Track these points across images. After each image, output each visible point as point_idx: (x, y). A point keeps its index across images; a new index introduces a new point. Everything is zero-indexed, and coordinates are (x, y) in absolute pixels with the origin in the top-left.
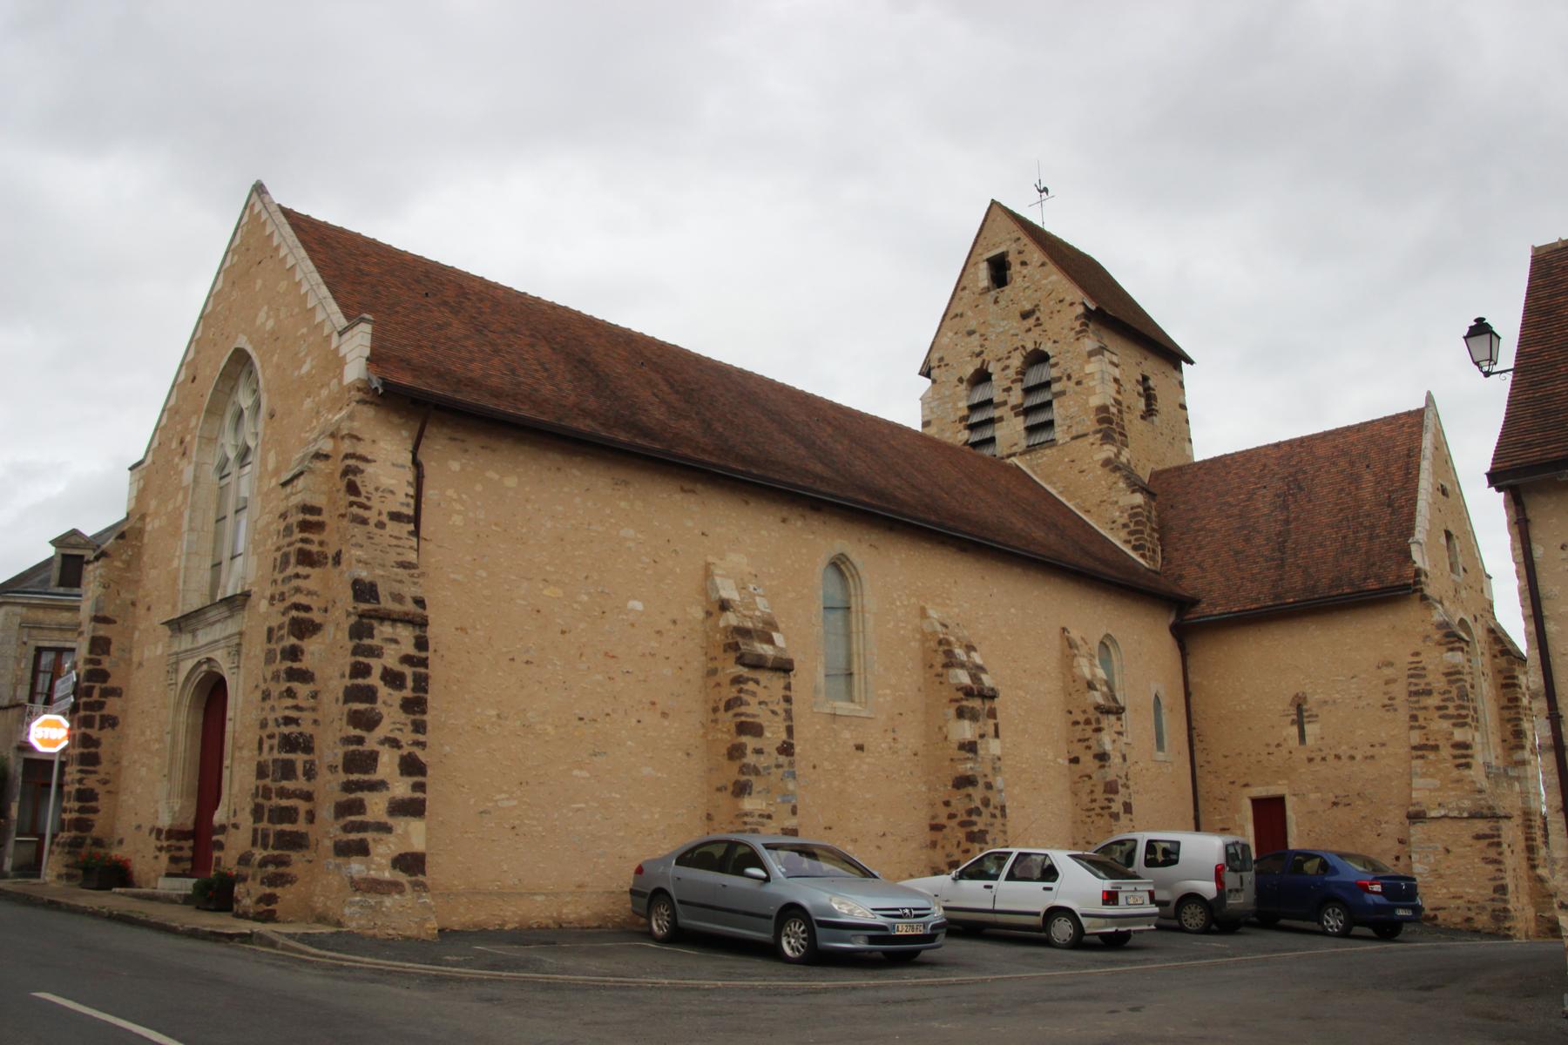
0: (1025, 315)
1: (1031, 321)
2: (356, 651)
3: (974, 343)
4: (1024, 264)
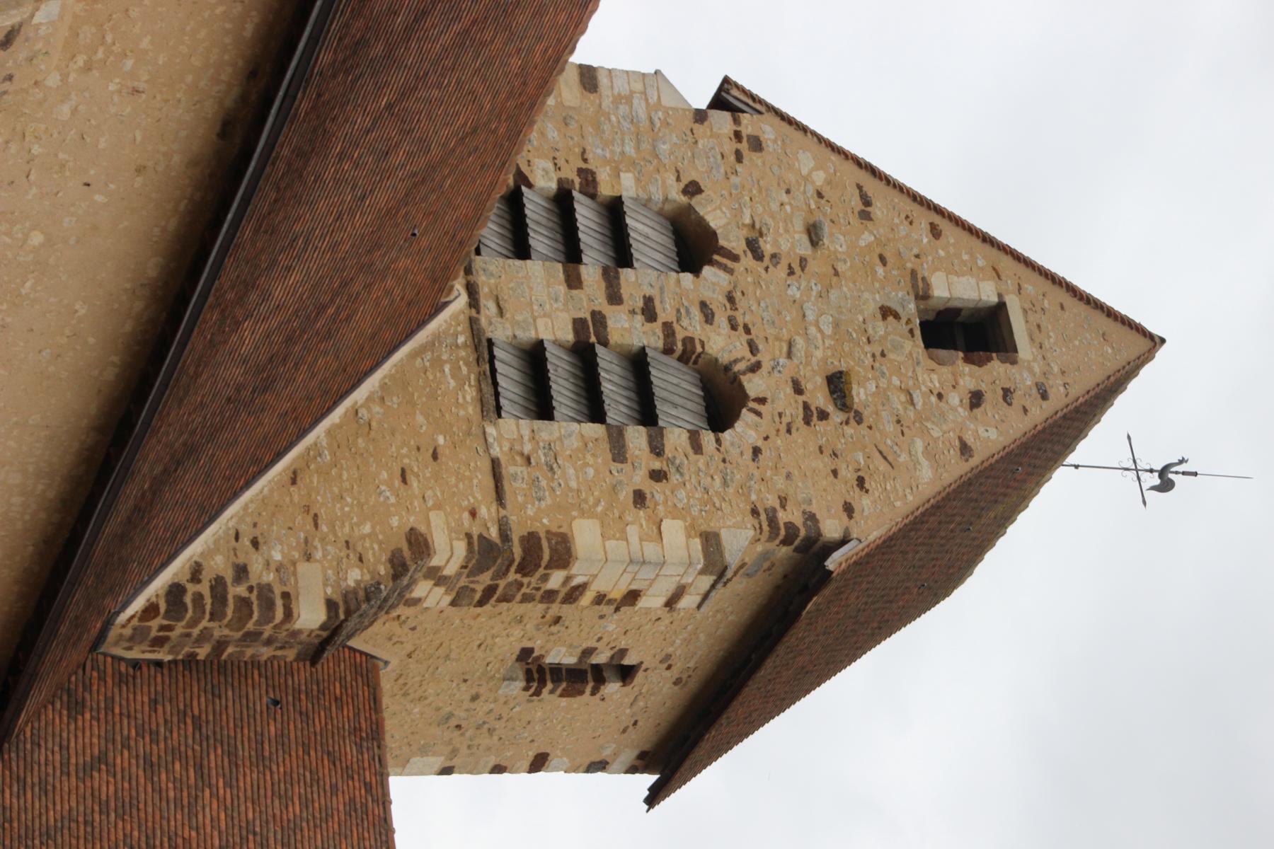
0: (837, 384)
1: (820, 398)
3: (787, 240)
4: (976, 399)
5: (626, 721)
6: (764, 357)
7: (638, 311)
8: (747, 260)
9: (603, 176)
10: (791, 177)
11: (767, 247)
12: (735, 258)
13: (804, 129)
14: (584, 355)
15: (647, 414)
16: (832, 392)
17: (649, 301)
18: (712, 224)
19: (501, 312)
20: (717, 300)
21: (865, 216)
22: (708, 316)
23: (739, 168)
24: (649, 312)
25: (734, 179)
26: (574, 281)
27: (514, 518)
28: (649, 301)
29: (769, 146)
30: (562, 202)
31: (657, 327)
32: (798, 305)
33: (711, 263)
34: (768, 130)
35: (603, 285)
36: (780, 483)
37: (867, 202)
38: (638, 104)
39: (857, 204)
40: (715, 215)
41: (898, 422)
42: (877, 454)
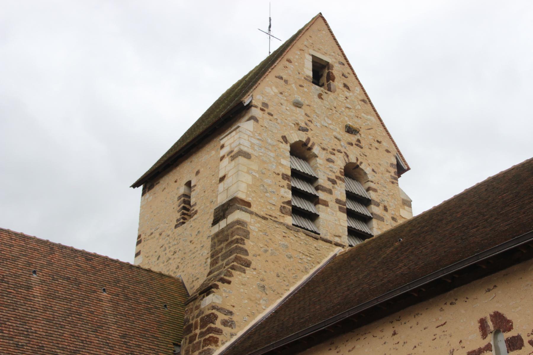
0: (350, 130)
1: (353, 138)
3: (299, 115)
4: (345, 86)
7: (333, 185)
8: (310, 134)
11: (303, 125)
12: (309, 139)
16: (352, 133)
17: (329, 179)
18: (298, 140)
19: (339, 237)
21: (286, 82)
23: (275, 117)
25: (279, 121)
27: (254, 263)
28: (329, 179)
30: (296, 192)
33: (310, 149)
35: (325, 193)
36: (382, 169)
37: (281, 78)
39: (282, 82)
40: (295, 137)
41: (357, 117)
42: (369, 131)
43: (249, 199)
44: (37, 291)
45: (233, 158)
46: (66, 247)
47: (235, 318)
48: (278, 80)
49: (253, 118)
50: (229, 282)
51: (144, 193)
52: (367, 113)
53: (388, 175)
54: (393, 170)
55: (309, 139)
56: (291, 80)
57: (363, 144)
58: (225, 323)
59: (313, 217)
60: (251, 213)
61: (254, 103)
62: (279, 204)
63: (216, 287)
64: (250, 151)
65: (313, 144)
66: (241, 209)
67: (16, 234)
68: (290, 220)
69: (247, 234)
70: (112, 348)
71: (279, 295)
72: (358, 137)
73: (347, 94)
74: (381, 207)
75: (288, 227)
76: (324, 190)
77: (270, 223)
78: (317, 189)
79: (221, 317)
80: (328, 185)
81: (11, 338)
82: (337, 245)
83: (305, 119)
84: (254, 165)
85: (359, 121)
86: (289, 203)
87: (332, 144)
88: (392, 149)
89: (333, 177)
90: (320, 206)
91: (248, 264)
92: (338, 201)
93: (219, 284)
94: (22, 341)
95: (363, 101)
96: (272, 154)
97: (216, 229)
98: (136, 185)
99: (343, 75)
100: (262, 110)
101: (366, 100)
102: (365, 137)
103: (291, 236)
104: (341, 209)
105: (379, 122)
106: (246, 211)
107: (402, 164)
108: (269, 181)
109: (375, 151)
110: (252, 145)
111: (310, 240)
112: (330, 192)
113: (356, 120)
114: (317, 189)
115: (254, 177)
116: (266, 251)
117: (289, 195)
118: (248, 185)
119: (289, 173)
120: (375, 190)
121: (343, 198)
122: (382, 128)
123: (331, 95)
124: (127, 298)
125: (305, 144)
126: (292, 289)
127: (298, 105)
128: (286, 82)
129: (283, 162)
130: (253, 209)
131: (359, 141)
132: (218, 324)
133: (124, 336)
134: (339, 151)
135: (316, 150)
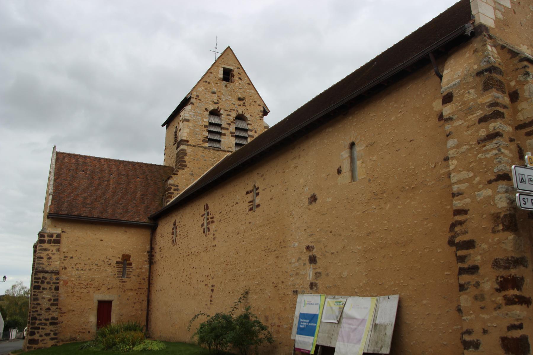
0: (240, 99)
1: (241, 103)
2: (58, 296)
3: (215, 98)
4: (240, 78)
5: (181, 131)
6: (235, 109)
8: (219, 105)
9: (205, 124)
10: (203, 93)
11: (216, 101)
12: (218, 107)
13: (194, 87)
14: (237, 137)
15: (246, 130)
17: (227, 124)
20: (226, 113)
21: (209, 83)
22: (229, 115)
24: (229, 124)
26: (225, 135)
28: (227, 124)
29: (198, 94)
30: (210, 132)
31: (232, 124)
32: (226, 100)
33: (219, 111)
34: (194, 95)
36: (256, 114)
37: (206, 82)
38: (191, 113)
39: (207, 84)
40: (211, 108)
43: (188, 139)
44: (111, 182)
45: (183, 122)
46: (126, 161)
47: (179, 188)
48: (205, 83)
49: (192, 104)
50: (177, 174)
51: (167, 127)
52: (250, 89)
53: (258, 116)
54: (261, 114)
55: (218, 107)
56: (211, 81)
57: (246, 104)
58: (175, 190)
59: (219, 141)
60: (188, 145)
61: (192, 96)
62: (203, 138)
63: (172, 177)
64: (189, 118)
65: (221, 109)
66: (183, 144)
67: (107, 159)
68: (207, 145)
69: (185, 154)
70: (136, 201)
71: (199, 176)
72: (244, 101)
73: (240, 82)
74: (253, 131)
75: (205, 148)
76: (224, 129)
77: (197, 148)
78: (221, 129)
79: (173, 188)
80: (226, 126)
81: (99, 201)
82: (229, 152)
83: (218, 98)
84: (190, 124)
85: (246, 94)
86: (207, 137)
87: (228, 107)
88: (262, 104)
89: (230, 122)
90: (222, 136)
91: (186, 166)
92: (231, 133)
93: (173, 176)
94: (103, 202)
95: (249, 84)
96: (200, 118)
97: (177, 152)
98: (163, 125)
99: (239, 73)
100: (196, 99)
101: (250, 83)
102: (247, 101)
103: (207, 152)
104: (232, 136)
105: (256, 92)
106: (185, 145)
107: (266, 110)
108: (198, 130)
109: (252, 107)
110: (190, 116)
111: (215, 152)
112: (227, 129)
113: (244, 93)
114: (221, 129)
115: (190, 129)
116: (194, 160)
117: (207, 134)
118: (188, 133)
119: (208, 124)
120: (251, 124)
121: (234, 131)
122: (257, 95)
123: (232, 84)
124: (147, 179)
125: (217, 110)
126: (205, 173)
127: (214, 93)
128: (209, 83)
129: (205, 120)
130: (190, 143)
131: (244, 103)
132: (172, 191)
133: (142, 195)
134: (234, 110)
135: (222, 112)
